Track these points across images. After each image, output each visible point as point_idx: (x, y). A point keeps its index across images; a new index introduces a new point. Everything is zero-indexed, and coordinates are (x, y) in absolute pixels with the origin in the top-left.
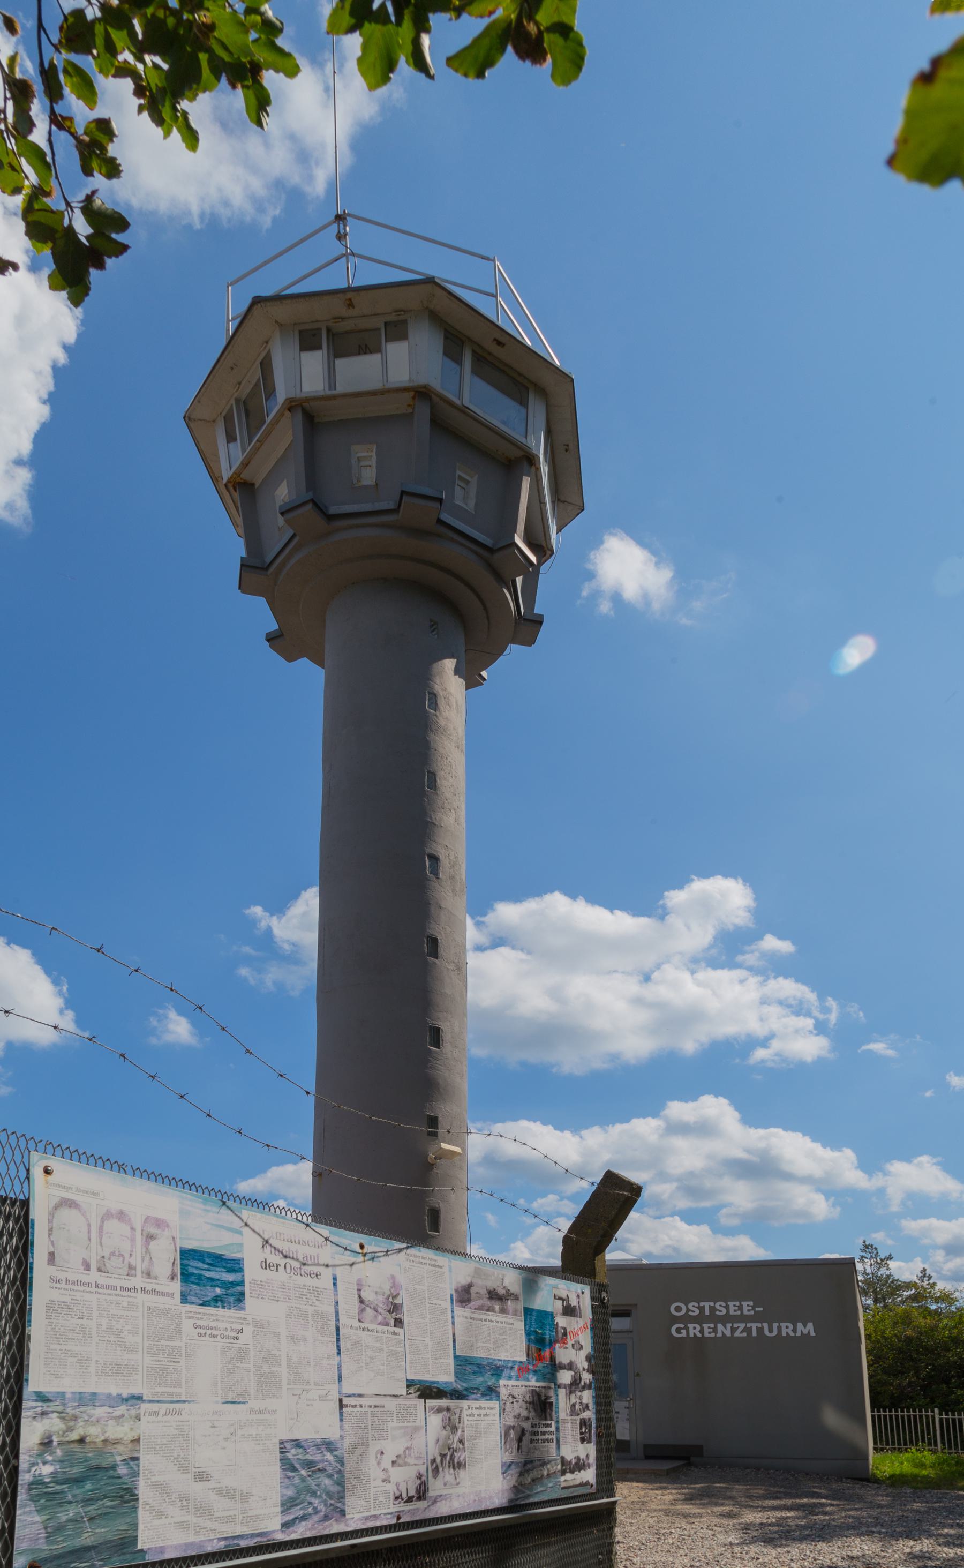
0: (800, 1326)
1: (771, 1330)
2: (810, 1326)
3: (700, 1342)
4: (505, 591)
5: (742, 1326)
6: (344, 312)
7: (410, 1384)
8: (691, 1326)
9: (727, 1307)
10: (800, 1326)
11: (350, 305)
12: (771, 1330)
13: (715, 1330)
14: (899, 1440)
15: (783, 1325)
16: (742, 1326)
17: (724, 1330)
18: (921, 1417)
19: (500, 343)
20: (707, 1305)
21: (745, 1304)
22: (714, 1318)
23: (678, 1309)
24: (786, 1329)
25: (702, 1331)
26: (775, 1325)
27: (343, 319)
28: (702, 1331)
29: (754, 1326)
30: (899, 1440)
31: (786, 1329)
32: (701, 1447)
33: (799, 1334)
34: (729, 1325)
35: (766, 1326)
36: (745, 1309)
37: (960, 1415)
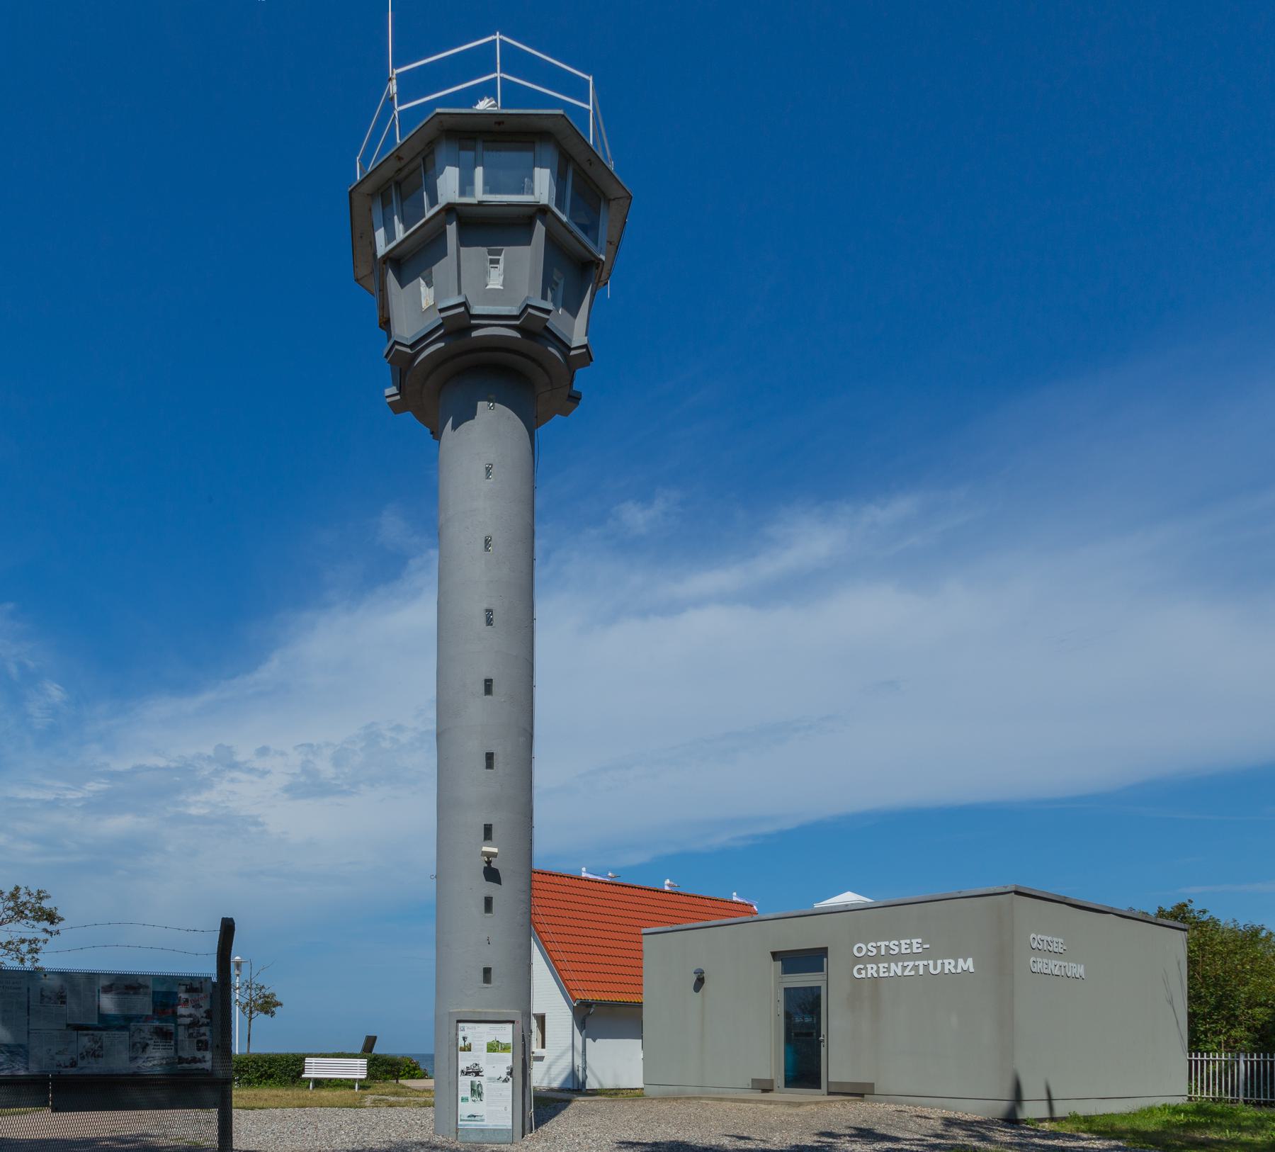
0: (961, 961)
1: (935, 968)
2: (970, 961)
3: (876, 980)
4: (475, 334)
5: (911, 964)
6: (400, 165)
7: (68, 1025)
8: (869, 966)
9: (899, 946)
10: (961, 961)
11: (400, 159)
12: (935, 968)
13: (888, 969)
14: (1265, 1091)
15: (946, 961)
16: (911, 964)
17: (896, 969)
18: (1265, 1063)
19: (499, 123)
20: (883, 944)
21: (914, 941)
22: (891, 958)
23: (860, 949)
24: (949, 965)
25: (878, 971)
26: (939, 962)
27: (400, 170)
28: (878, 971)
29: (921, 963)
30: (1265, 1091)
31: (949, 965)
32: (872, 1085)
33: (959, 970)
34: (900, 964)
35: (931, 962)
36: (915, 946)
37: (1272, 1057)
